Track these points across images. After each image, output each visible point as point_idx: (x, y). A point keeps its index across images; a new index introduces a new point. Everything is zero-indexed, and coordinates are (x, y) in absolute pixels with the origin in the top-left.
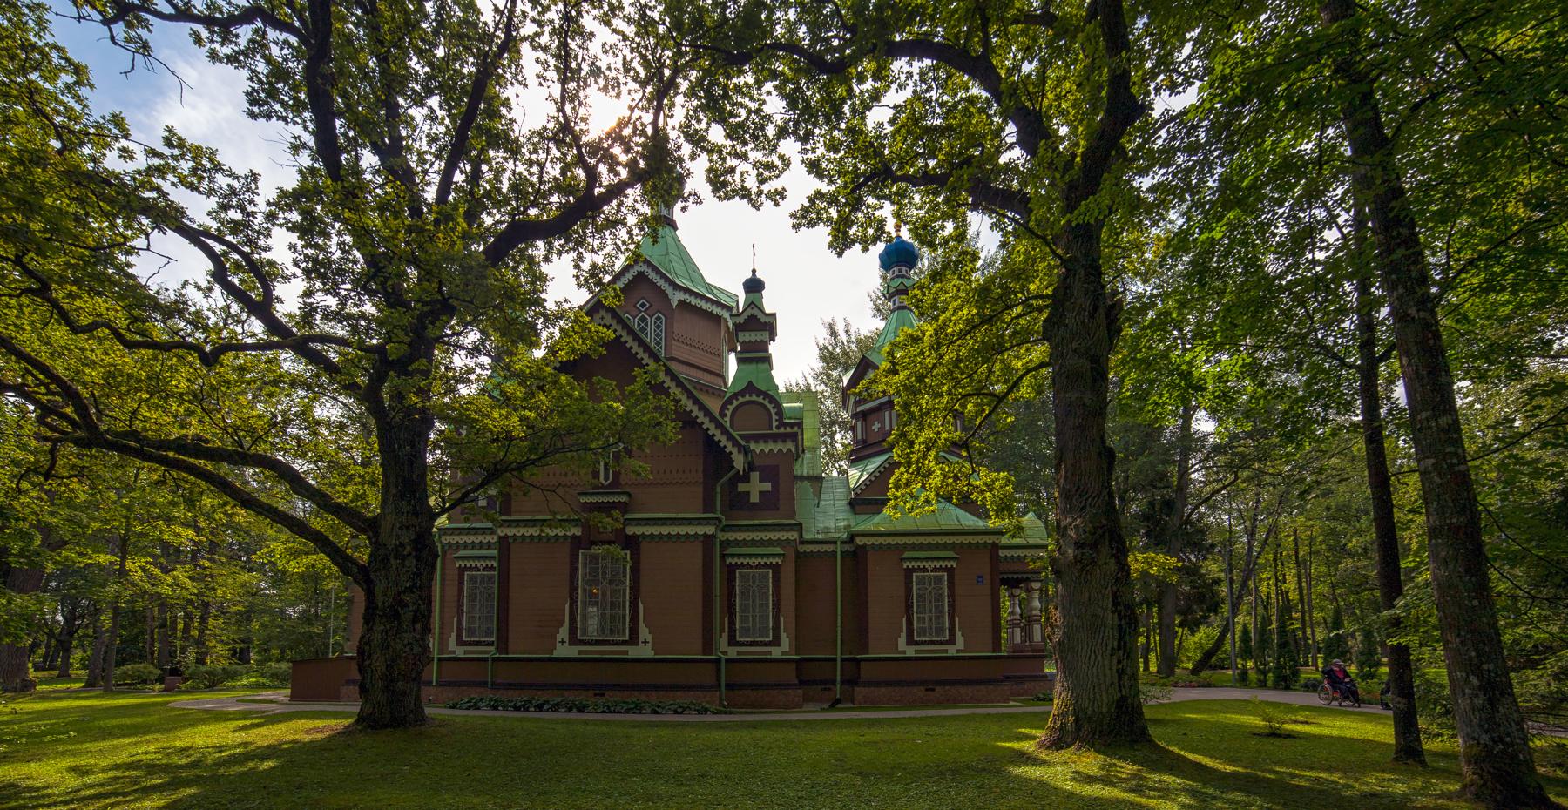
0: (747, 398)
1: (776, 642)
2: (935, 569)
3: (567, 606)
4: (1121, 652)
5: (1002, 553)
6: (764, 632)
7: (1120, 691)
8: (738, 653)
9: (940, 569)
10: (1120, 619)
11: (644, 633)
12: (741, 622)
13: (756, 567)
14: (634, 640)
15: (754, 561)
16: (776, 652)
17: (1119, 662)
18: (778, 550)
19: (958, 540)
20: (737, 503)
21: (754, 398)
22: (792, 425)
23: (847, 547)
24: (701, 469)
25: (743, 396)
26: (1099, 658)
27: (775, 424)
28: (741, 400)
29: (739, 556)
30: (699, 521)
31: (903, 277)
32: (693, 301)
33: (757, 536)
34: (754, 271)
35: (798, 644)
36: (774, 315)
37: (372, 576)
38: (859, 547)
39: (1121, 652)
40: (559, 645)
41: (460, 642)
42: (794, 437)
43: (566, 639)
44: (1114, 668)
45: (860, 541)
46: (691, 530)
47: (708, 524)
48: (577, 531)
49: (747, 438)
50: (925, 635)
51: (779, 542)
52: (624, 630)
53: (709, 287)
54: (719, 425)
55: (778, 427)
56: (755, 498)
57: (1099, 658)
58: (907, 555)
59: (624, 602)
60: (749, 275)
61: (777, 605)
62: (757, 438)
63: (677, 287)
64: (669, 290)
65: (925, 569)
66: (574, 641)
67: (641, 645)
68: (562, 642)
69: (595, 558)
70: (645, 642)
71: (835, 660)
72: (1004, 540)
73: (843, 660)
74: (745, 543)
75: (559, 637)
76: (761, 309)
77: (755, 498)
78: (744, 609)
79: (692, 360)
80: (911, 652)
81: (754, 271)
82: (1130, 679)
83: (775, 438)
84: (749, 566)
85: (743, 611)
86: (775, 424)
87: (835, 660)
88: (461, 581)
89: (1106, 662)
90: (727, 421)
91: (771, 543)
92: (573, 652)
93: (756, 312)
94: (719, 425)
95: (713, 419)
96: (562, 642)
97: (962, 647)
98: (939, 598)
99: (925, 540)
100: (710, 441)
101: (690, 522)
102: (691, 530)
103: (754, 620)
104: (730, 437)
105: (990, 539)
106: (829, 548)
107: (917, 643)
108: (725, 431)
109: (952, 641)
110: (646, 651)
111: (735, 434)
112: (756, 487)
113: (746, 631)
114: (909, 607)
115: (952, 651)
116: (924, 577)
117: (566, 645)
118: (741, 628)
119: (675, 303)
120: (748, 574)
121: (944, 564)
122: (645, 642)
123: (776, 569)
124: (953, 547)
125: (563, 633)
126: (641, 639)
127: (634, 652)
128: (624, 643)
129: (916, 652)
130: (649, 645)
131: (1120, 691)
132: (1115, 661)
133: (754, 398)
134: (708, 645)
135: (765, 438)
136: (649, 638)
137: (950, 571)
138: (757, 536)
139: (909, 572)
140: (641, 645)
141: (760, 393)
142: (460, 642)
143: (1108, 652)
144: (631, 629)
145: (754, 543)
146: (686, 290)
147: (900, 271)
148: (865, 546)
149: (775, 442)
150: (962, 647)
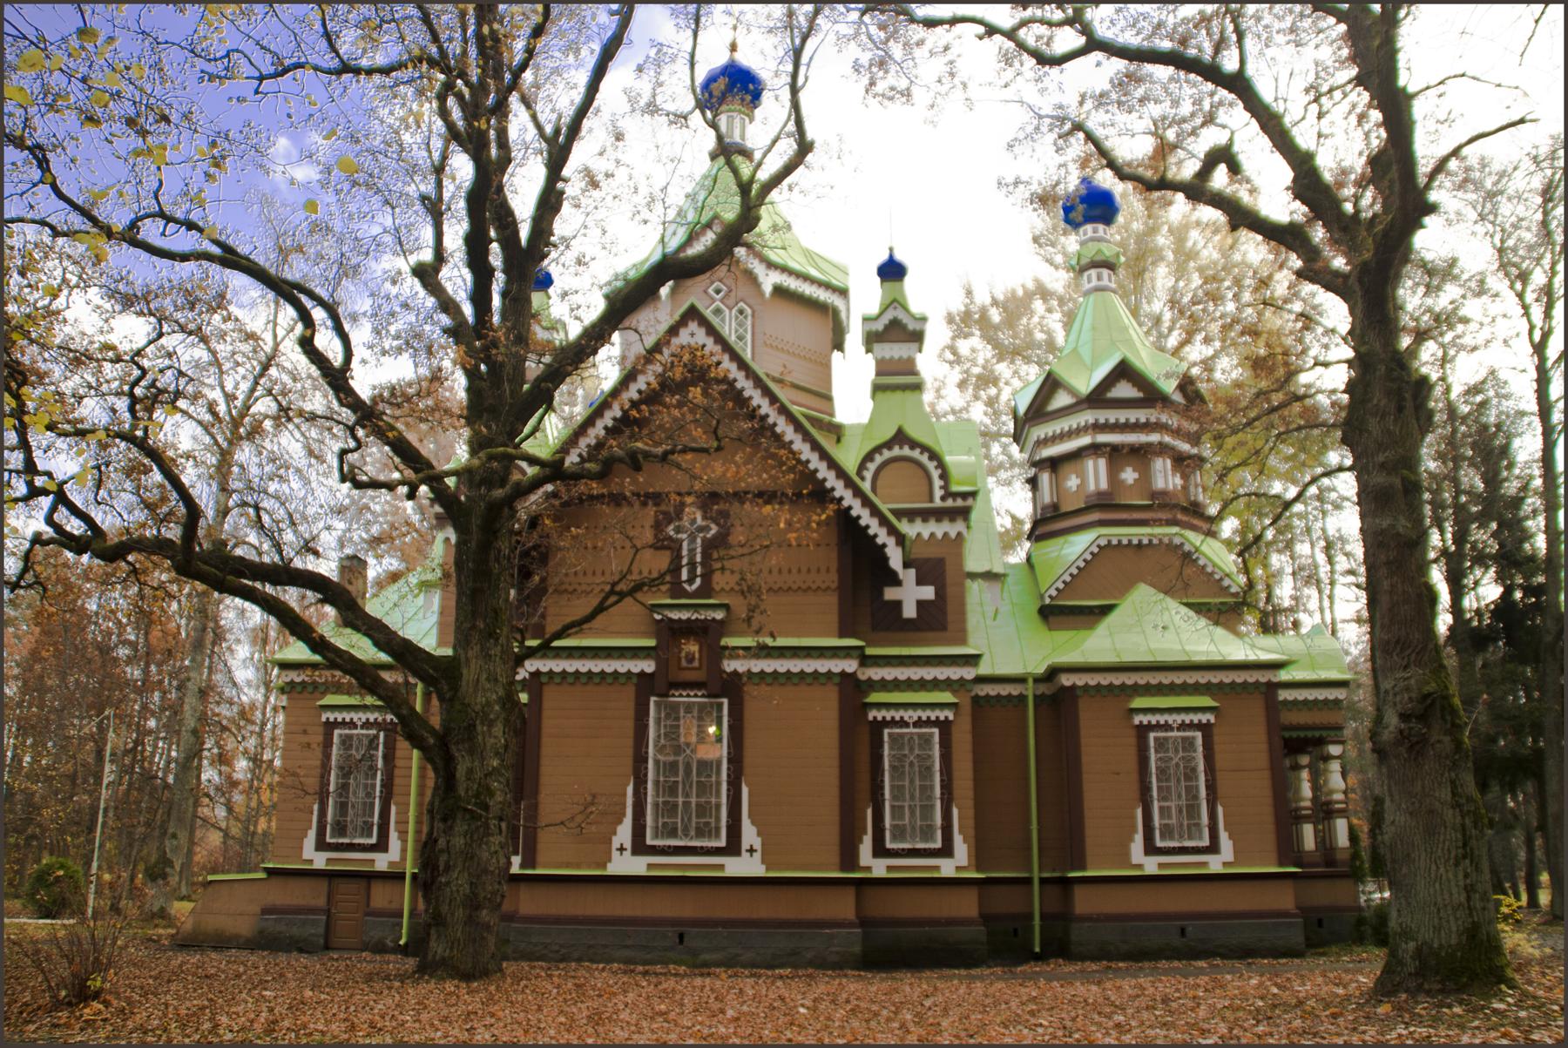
0: (896, 451)
1: (946, 851)
2: (1183, 726)
3: (630, 790)
4: (1467, 861)
5: (1284, 695)
6: (927, 833)
7: (1471, 915)
8: (890, 868)
9: (928, 723)
10: (1463, 817)
11: (750, 835)
12: (893, 817)
13: (916, 724)
14: (733, 847)
15: (911, 715)
16: (946, 868)
17: (1466, 876)
18: (947, 697)
19: (1216, 677)
20: (888, 620)
21: (906, 451)
22: (965, 496)
23: (1043, 689)
24: (834, 566)
25: (890, 448)
26: (1442, 870)
27: (938, 493)
28: (887, 454)
29: (888, 706)
30: (834, 652)
31: (1099, 240)
32: (793, 284)
33: (915, 673)
34: (891, 250)
35: (980, 857)
36: (924, 319)
37: (453, 748)
38: (1063, 688)
39: (1467, 861)
40: (615, 854)
41: (1151, 849)
42: (964, 513)
43: (628, 845)
44: (1461, 883)
45: (1066, 680)
46: (823, 666)
47: (848, 656)
48: (648, 666)
49: (899, 514)
50: (1172, 838)
51: (947, 684)
52: (718, 829)
53: (809, 255)
54: (858, 493)
55: (943, 498)
56: (910, 611)
57: (1442, 870)
58: (1138, 703)
59: (718, 784)
60: (884, 257)
61: (947, 787)
62: (911, 515)
63: (771, 265)
64: (759, 269)
65: (1167, 727)
66: (640, 847)
67: (745, 855)
68: (622, 849)
69: (674, 708)
70: (751, 850)
71: (1028, 881)
72: (1284, 676)
73: (1043, 881)
74: (896, 685)
75: (616, 843)
76: (905, 309)
77: (910, 611)
78: (898, 792)
79: (818, 399)
80: (1151, 866)
81: (891, 250)
82: (1482, 899)
83: (939, 514)
84: (903, 723)
85: (894, 797)
86: (938, 493)
87: (1028, 881)
88: (328, 744)
89: (1451, 875)
90: (866, 486)
91: (935, 684)
92: (637, 866)
93: (901, 315)
94: (858, 493)
95: (849, 483)
96: (622, 849)
97: (965, 863)
98: (1191, 774)
99: (1166, 678)
100: (846, 521)
101: (821, 652)
102: (823, 666)
103: (912, 813)
104: (876, 512)
105: (1263, 677)
106: (1014, 690)
107: (654, 851)
108: (867, 502)
109: (1213, 848)
110: (745, 866)
111: (884, 508)
112: (911, 594)
113: (899, 833)
114: (1145, 790)
115: (1215, 864)
116: (1166, 739)
117: (628, 853)
118: (894, 827)
119: (768, 289)
120: (902, 736)
121: (1196, 718)
122: (751, 850)
123: (944, 726)
124: (1207, 689)
125: (624, 834)
126: (745, 845)
127: (736, 867)
128: (718, 852)
129: (1161, 866)
130: (758, 855)
131: (1471, 915)
132: (1461, 876)
133: (906, 451)
134: (849, 857)
135: (926, 515)
136: (757, 844)
137: (1205, 728)
138: (915, 673)
139: (1144, 730)
140: (745, 855)
141: (914, 444)
142: (1151, 849)
143: (1452, 861)
144: (729, 827)
145: (909, 685)
146: (784, 269)
147: (1095, 231)
148: (1073, 687)
149: (939, 520)
150: (965, 863)
